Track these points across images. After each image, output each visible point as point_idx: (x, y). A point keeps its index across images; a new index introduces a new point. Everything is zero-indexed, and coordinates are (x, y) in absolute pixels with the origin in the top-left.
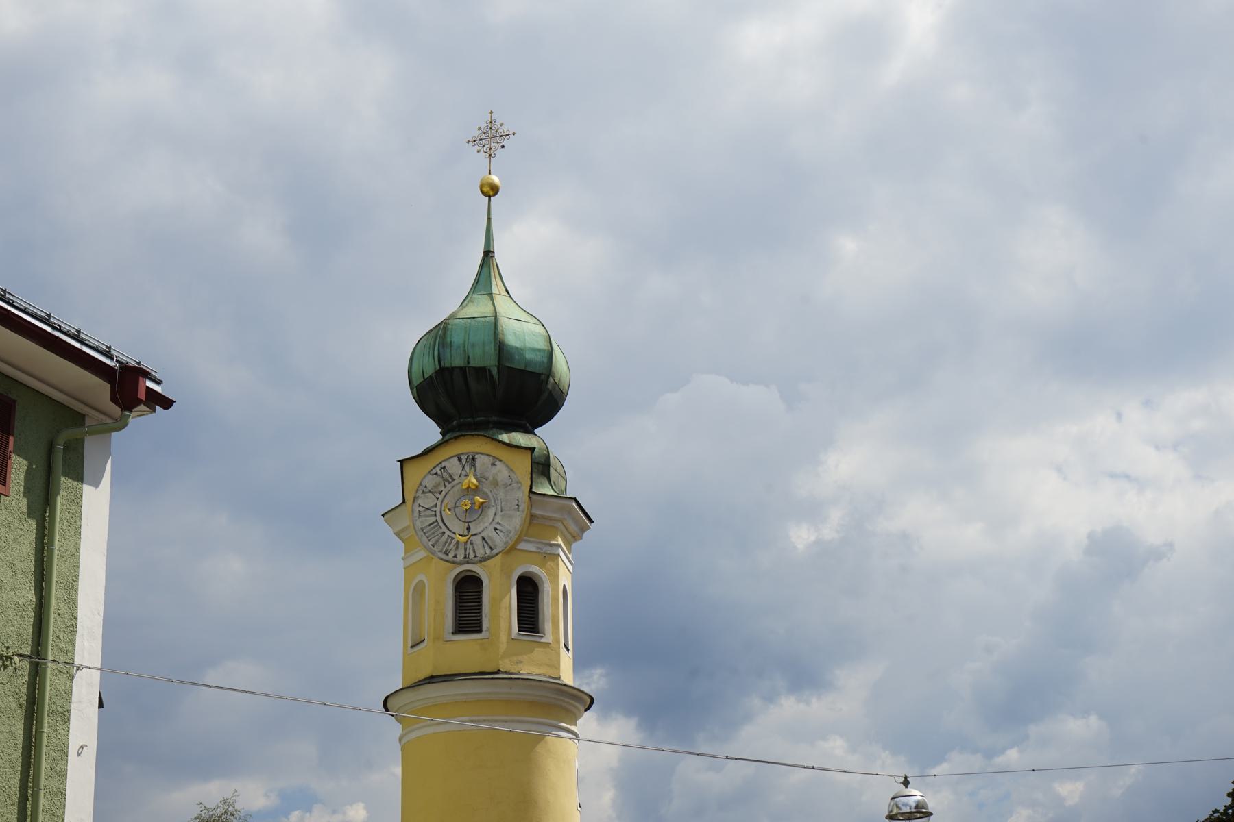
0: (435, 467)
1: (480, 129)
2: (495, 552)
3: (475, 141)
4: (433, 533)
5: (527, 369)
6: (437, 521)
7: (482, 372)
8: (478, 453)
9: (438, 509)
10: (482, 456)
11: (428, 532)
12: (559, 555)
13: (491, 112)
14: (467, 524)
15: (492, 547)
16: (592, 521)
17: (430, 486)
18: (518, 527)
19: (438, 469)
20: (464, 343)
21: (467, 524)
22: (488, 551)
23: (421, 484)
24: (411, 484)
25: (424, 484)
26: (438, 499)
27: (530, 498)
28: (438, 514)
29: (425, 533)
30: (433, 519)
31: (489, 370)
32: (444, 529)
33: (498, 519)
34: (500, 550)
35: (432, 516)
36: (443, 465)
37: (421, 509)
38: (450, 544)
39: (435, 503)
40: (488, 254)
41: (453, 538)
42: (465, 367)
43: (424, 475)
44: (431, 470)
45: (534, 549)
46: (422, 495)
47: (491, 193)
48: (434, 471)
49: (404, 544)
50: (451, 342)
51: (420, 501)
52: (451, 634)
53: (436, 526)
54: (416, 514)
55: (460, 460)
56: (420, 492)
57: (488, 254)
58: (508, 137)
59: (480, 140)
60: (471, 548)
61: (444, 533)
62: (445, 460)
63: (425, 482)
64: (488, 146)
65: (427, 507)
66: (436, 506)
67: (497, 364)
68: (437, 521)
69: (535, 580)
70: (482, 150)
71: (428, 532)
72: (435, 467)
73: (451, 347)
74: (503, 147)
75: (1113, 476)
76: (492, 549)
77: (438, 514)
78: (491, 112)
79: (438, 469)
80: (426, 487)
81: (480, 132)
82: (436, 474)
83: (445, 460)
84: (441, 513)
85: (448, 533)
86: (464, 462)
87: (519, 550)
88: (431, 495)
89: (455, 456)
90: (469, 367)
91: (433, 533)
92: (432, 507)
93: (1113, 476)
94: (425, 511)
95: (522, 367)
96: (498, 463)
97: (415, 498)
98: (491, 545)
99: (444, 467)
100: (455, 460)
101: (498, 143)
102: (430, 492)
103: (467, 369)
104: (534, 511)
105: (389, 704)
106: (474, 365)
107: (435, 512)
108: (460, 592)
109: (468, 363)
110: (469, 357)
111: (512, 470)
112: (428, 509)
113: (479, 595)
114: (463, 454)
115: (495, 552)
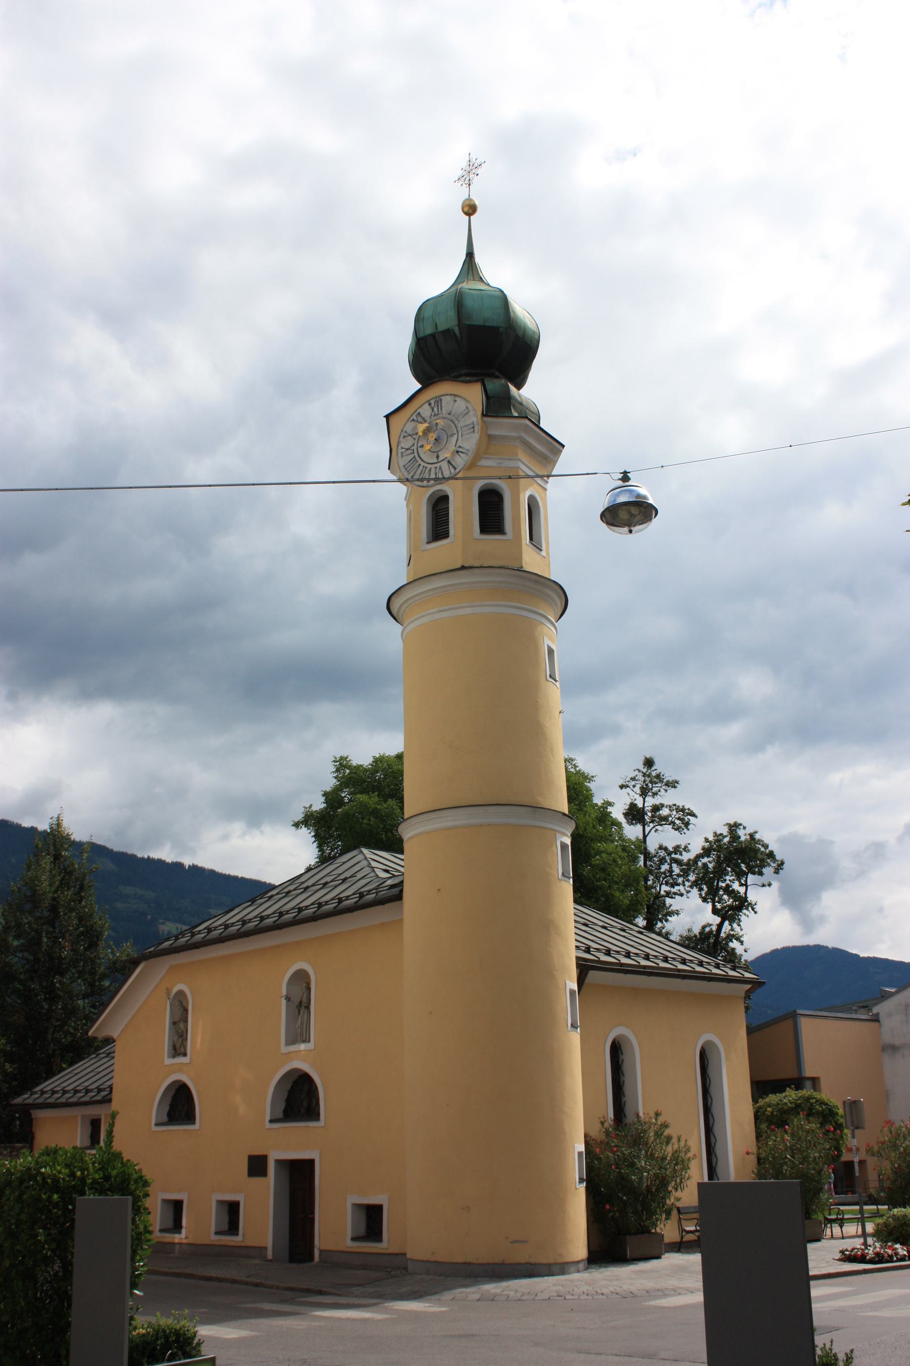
0: (412, 415)
1: (462, 169)
2: (457, 470)
3: (459, 179)
4: (412, 467)
5: (486, 324)
6: (414, 457)
7: (447, 332)
8: (442, 396)
9: (415, 448)
10: (447, 397)
11: (408, 467)
12: (519, 467)
13: (470, 154)
14: (436, 453)
15: (456, 467)
16: (563, 446)
17: (409, 431)
18: (474, 446)
19: (414, 416)
20: (433, 316)
21: (436, 453)
22: (452, 470)
23: (402, 431)
24: (395, 432)
25: (404, 430)
26: (415, 439)
27: (484, 422)
28: (415, 451)
29: (406, 469)
30: (412, 456)
31: (453, 330)
32: (420, 461)
33: (459, 443)
34: (461, 468)
35: (411, 454)
36: (418, 411)
37: (404, 450)
38: (424, 473)
39: (413, 443)
40: (470, 255)
41: (426, 468)
42: (435, 333)
43: (404, 423)
44: (410, 418)
45: (495, 464)
46: (404, 439)
47: (470, 212)
48: (412, 419)
49: (406, 487)
50: (423, 317)
51: (402, 445)
52: (426, 544)
53: (415, 460)
54: (400, 455)
55: (430, 404)
56: (402, 437)
57: (470, 255)
58: (480, 166)
59: (463, 176)
60: (440, 472)
61: (420, 465)
62: (419, 408)
63: (406, 429)
64: (468, 179)
65: (407, 448)
66: (413, 445)
67: (457, 323)
68: (414, 457)
69: (499, 491)
70: (464, 184)
71: (408, 467)
72: (412, 415)
73: (423, 321)
74: (477, 175)
75: (662, 1359)
76: (455, 469)
77: (415, 451)
78: (470, 154)
79: (414, 416)
80: (406, 432)
81: (463, 171)
82: (413, 420)
83: (419, 408)
84: (417, 449)
85: (423, 464)
86: (433, 405)
87: (481, 466)
88: (410, 437)
89: (426, 402)
90: (438, 332)
91: (412, 467)
92: (411, 447)
93: (662, 1359)
94: (406, 451)
95: (481, 323)
96: (457, 399)
97: (399, 443)
98: (455, 465)
99: (419, 414)
100: (426, 406)
101: (474, 173)
102: (409, 435)
103: (436, 334)
104: (490, 432)
105: (395, 608)
106: (440, 330)
107: (413, 450)
108: (436, 511)
109: (437, 328)
110: (436, 324)
111: (468, 401)
112: (408, 449)
113: (499, 522)
114: (431, 399)
115: (457, 470)
